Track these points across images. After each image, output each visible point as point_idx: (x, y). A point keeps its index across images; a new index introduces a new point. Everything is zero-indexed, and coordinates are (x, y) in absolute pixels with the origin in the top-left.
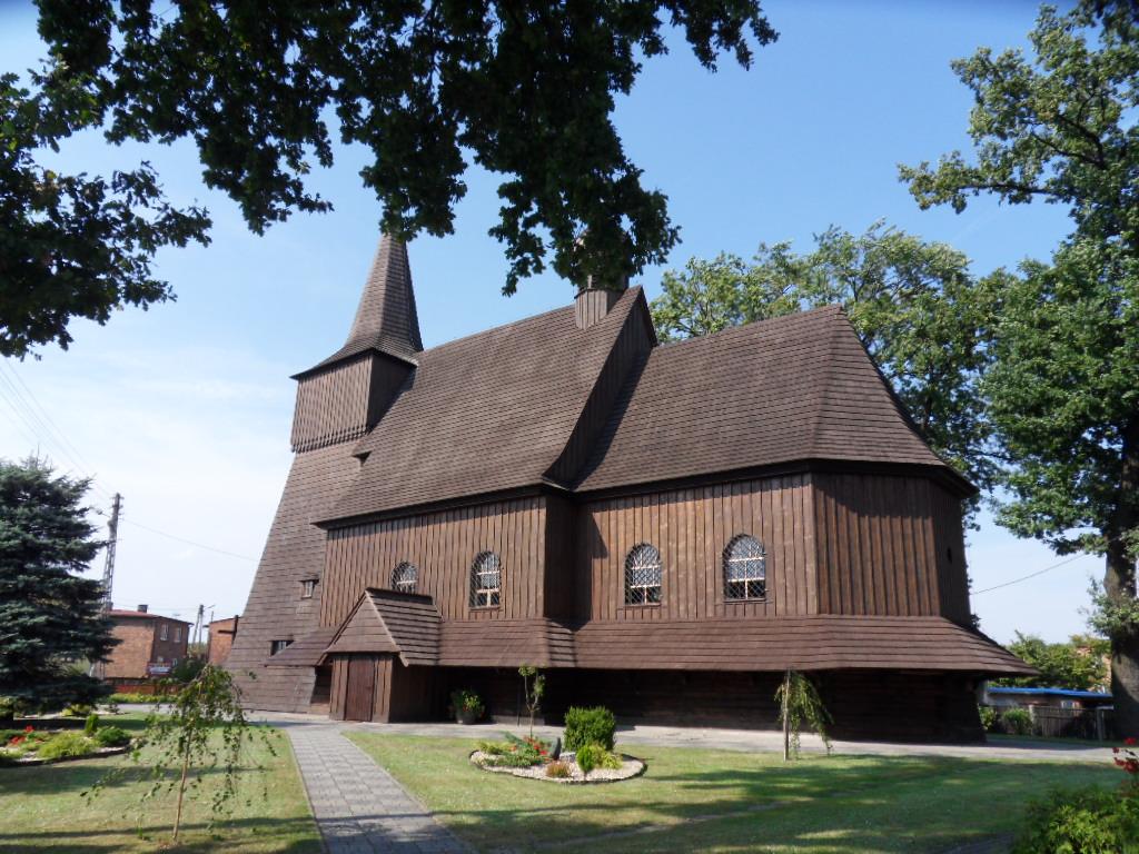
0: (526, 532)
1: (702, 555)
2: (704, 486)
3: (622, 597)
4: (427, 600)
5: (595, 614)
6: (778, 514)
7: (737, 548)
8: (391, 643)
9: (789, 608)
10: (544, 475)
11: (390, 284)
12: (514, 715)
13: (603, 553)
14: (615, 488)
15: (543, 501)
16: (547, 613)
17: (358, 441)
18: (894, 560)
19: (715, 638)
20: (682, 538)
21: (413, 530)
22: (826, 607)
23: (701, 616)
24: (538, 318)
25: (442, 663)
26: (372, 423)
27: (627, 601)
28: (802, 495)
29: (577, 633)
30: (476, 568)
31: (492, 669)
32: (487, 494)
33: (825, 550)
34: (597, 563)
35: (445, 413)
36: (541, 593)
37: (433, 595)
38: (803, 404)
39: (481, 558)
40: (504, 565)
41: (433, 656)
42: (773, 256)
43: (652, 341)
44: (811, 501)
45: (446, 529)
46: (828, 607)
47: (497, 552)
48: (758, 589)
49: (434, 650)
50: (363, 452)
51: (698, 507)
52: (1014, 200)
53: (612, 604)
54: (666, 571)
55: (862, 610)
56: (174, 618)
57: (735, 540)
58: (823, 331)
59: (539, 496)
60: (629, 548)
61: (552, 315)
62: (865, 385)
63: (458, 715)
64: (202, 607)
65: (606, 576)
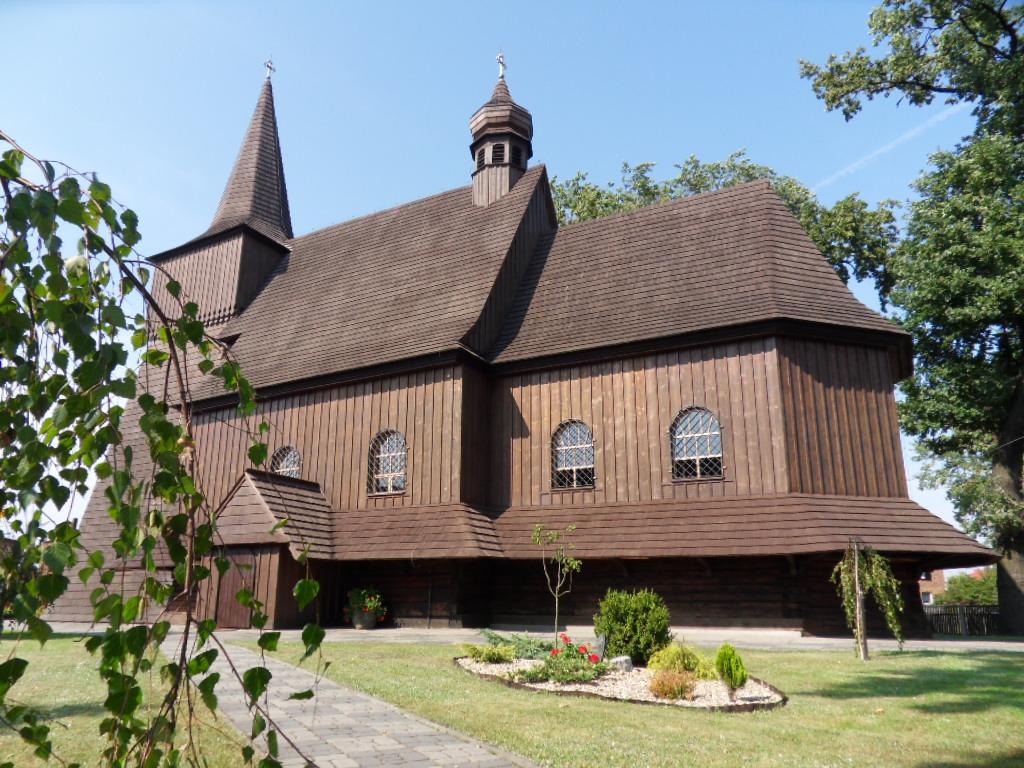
0: (438, 407)
1: (644, 431)
2: (646, 355)
3: (547, 481)
4: (314, 487)
5: (515, 502)
6: (735, 383)
7: (688, 420)
8: (282, 536)
9: (752, 486)
10: (461, 341)
12: (424, 616)
13: (524, 432)
14: (540, 358)
15: (459, 371)
16: (463, 499)
17: (225, 325)
18: (861, 436)
19: (670, 521)
20: (618, 412)
21: (296, 410)
22: (797, 486)
23: (644, 498)
24: (427, 200)
25: (337, 557)
26: (241, 307)
27: (553, 485)
28: (768, 360)
29: (496, 521)
30: (374, 450)
31: (406, 562)
32: (386, 364)
33: (793, 423)
34: (516, 443)
35: (327, 291)
36: (457, 475)
37: (321, 483)
38: (749, 270)
41: (328, 550)
42: (636, 178)
43: (553, 222)
45: (335, 409)
46: (799, 486)
47: (402, 429)
48: (712, 467)
49: (328, 542)
51: (638, 378)
52: (917, 100)
53: (536, 488)
54: (600, 450)
55: (833, 490)
57: (683, 413)
58: (754, 204)
59: (454, 365)
60: (555, 425)
61: (445, 196)
62: (807, 255)
63: (355, 619)
65: (526, 458)
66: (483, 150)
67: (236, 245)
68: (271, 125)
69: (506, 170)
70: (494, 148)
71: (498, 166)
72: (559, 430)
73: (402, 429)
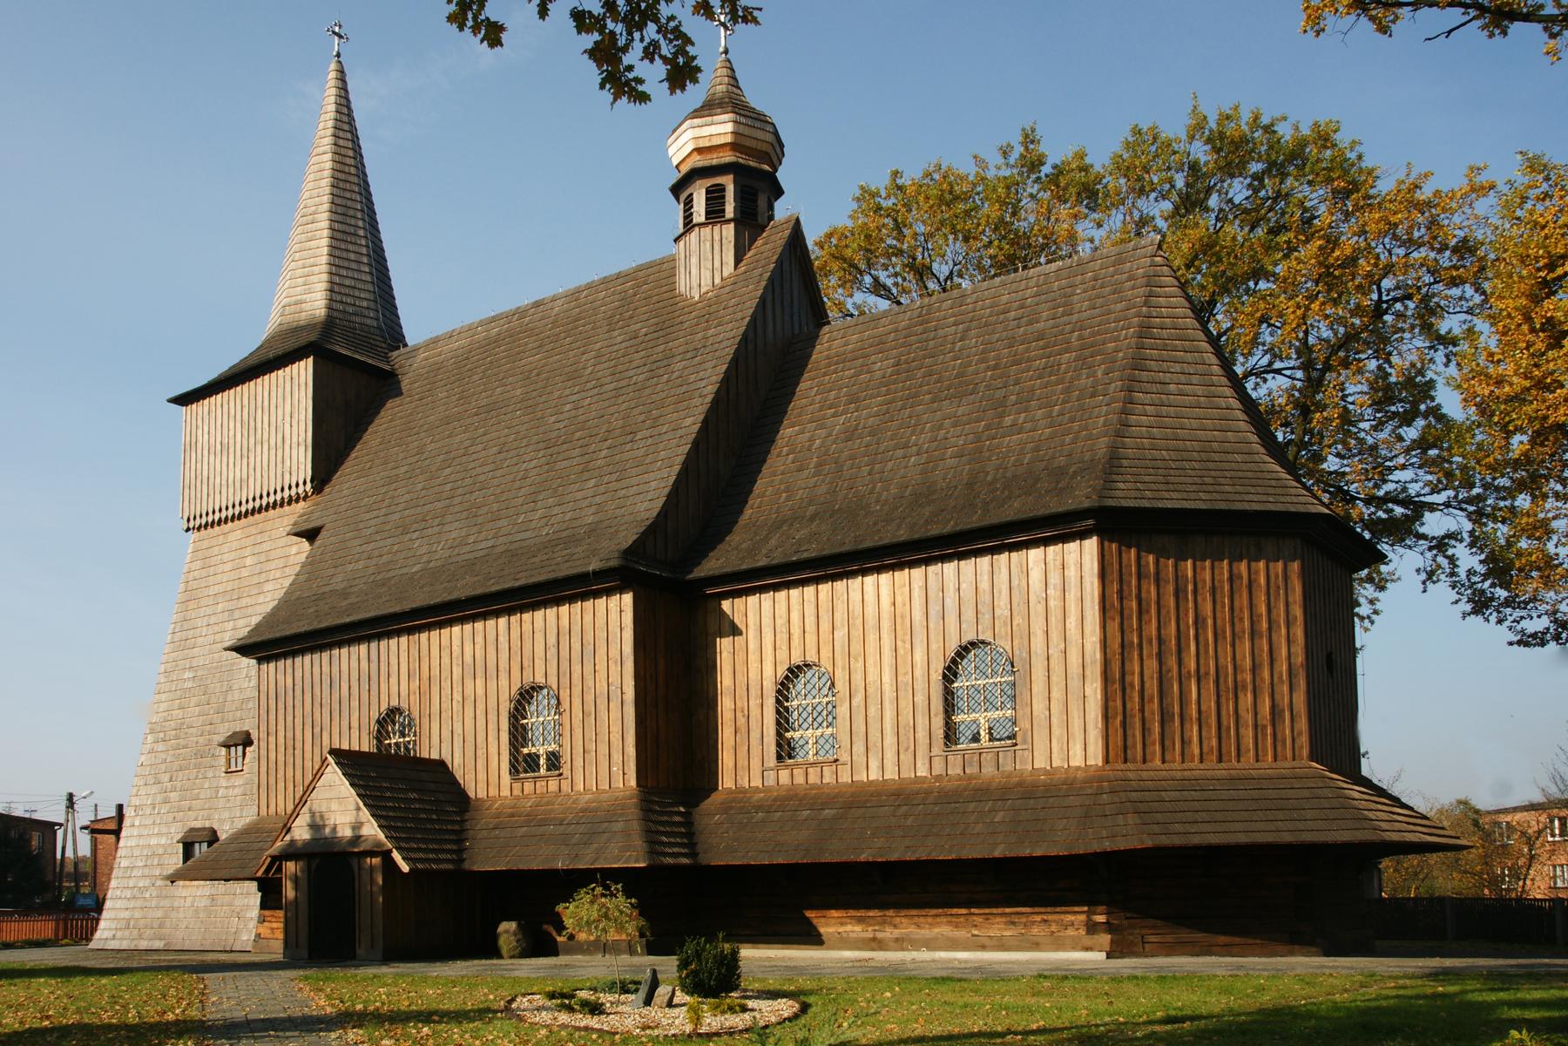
7: (967, 665)
11: (336, 226)
39: (526, 695)
40: (565, 705)
44: (1096, 581)
50: (311, 526)
56: (27, 815)
60: (782, 671)
64: (71, 797)
66: (691, 194)
67: (303, 371)
68: (351, 153)
69: (729, 231)
70: (708, 192)
71: (714, 224)
72: (787, 677)
73: (553, 682)
